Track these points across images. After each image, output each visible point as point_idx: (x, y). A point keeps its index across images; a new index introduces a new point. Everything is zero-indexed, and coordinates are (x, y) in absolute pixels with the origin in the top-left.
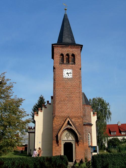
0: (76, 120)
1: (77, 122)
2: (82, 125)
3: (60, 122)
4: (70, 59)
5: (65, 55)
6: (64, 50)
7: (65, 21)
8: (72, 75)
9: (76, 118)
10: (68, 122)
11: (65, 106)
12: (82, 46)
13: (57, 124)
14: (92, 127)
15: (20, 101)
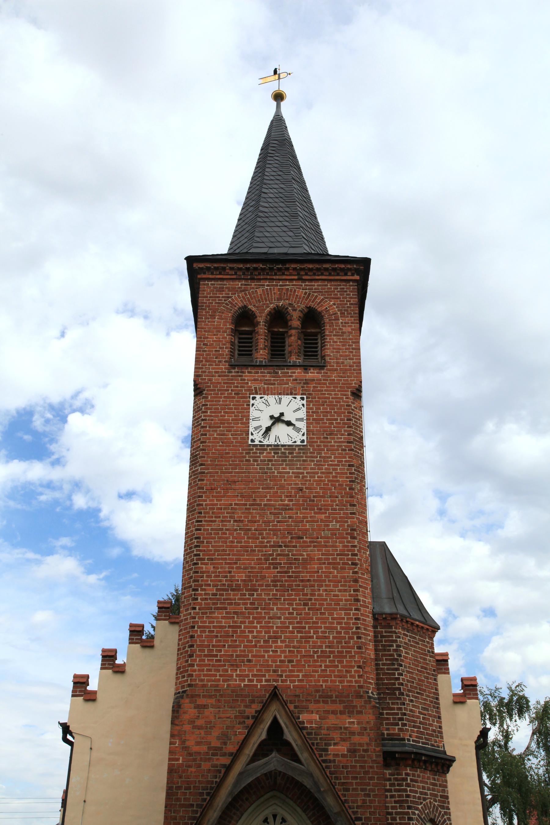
0: (332, 720)
1: (336, 736)
2: (375, 752)
3: (216, 733)
4: (293, 340)
5: (261, 319)
6: (260, 291)
8: (304, 430)
9: (330, 707)
10: (275, 728)
11: (259, 619)
12: (366, 262)
14: (449, 776)
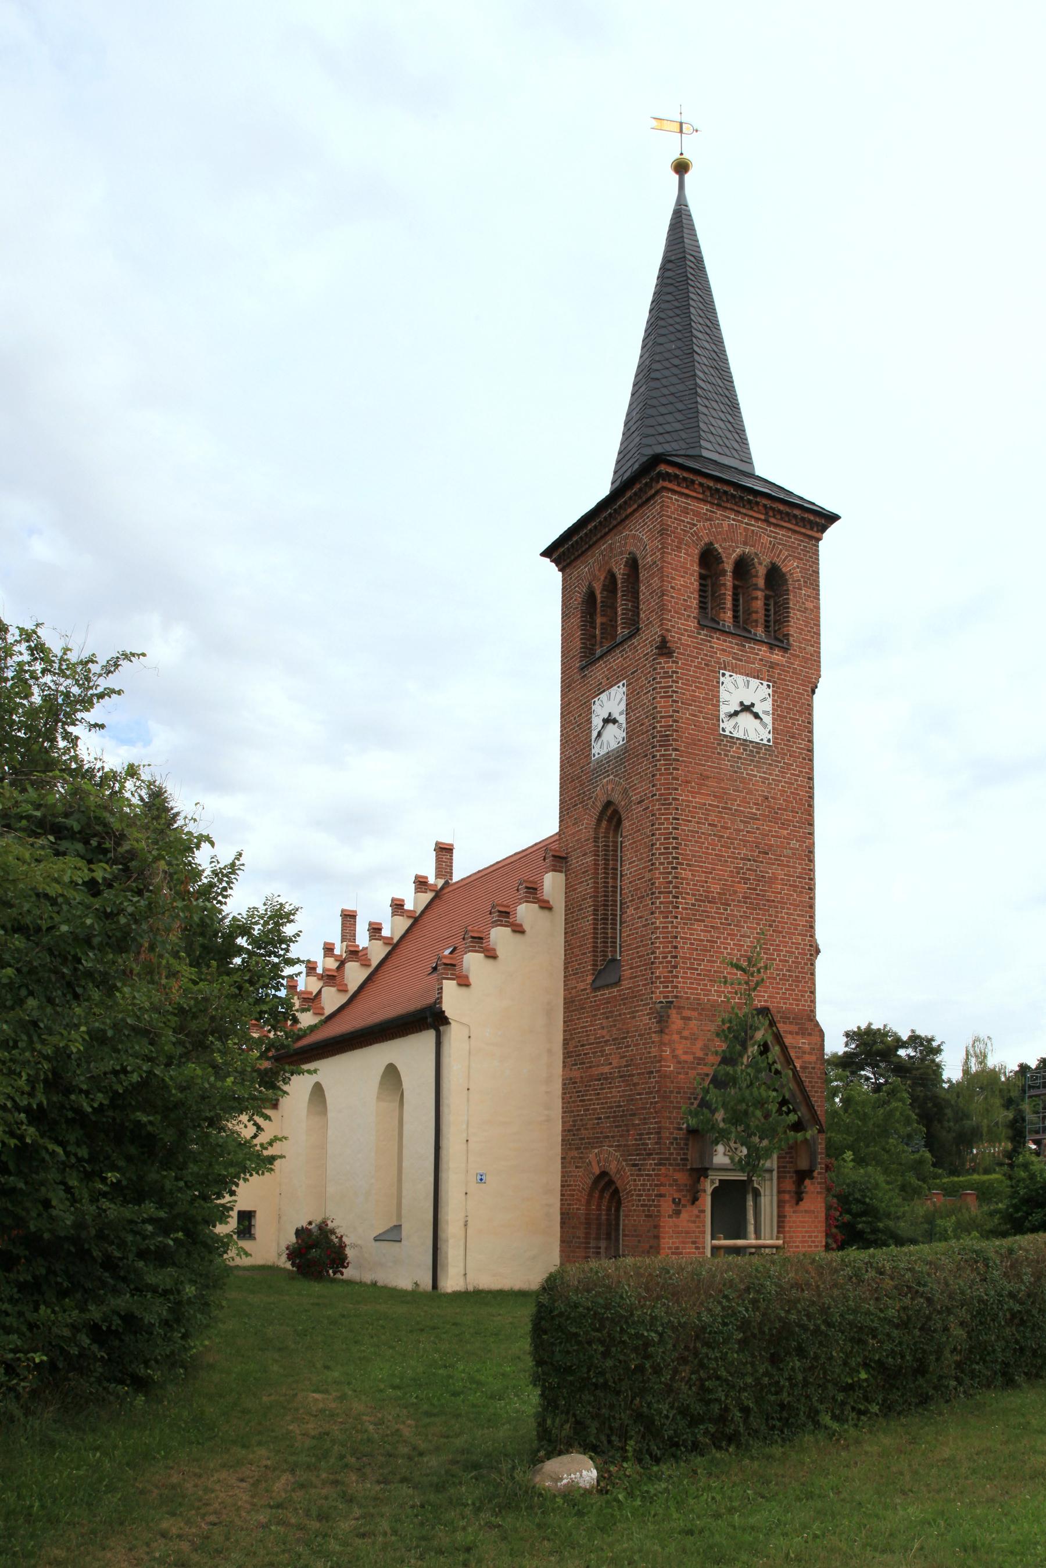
3: (699, 1044)
7: (681, 225)
13: (684, 1057)
15: (870, 1024)
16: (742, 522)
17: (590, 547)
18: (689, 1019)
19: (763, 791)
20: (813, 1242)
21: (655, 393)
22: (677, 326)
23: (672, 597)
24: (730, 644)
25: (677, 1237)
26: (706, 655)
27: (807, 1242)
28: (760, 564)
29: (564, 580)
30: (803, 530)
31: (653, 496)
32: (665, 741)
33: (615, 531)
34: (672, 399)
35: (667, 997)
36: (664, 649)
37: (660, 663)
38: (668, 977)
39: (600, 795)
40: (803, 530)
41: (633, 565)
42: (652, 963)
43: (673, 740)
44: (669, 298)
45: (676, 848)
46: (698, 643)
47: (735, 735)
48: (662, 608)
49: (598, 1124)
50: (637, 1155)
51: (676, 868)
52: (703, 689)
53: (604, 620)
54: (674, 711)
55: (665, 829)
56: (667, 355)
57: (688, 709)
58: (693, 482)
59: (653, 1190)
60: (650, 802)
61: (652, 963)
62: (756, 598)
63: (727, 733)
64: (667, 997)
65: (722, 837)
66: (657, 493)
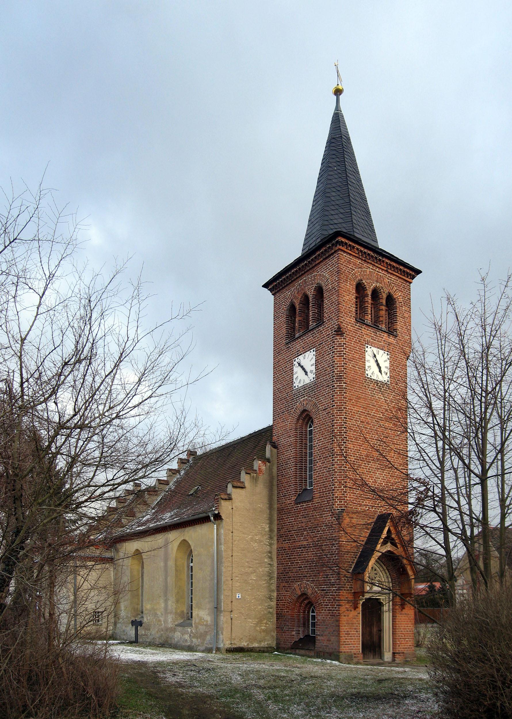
7: (337, 121)
16: (375, 270)
17: (292, 281)
18: (352, 518)
19: (385, 406)
20: (409, 629)
21: (327, 204)
22: (339, 171)
23: (344, 305)
24: (370, 331)
25: (348, 626)
26: (359, 336)
27: (406, 629)
28: (384, 292)
29: (275, 299)
30: (404, 277)
31: (332, 254)
32: (340, 378)
33: (308, 273)
34: (337, 207)
35: (342, 507)
36: (339, 332)
37: (337, 339)
38: (342, 497)
39: (299, 407)
40: (404, 277)
41: (320, 291)
42: (333, 490)
43: (344, 378)
44: (334, 157)
45: (346, 433)
46: (355, 330)
47: (372, 378)
48: (339, 310)
49: (300, 570)
50: (325, 585)
51: (346, 443)
52: (358, 353)
53: (301, 318)
54: (344, 364)
55: (339, 423)
56: (334, 185)
57: (351, 363)
58: (354, 247)
59: (335, 603)
60: (331, 410)
61: (333, 490)
62: (382, 310)
63: (369, 376)
64: (342, 507)
65: (367, 428)
66: (335, 252)
